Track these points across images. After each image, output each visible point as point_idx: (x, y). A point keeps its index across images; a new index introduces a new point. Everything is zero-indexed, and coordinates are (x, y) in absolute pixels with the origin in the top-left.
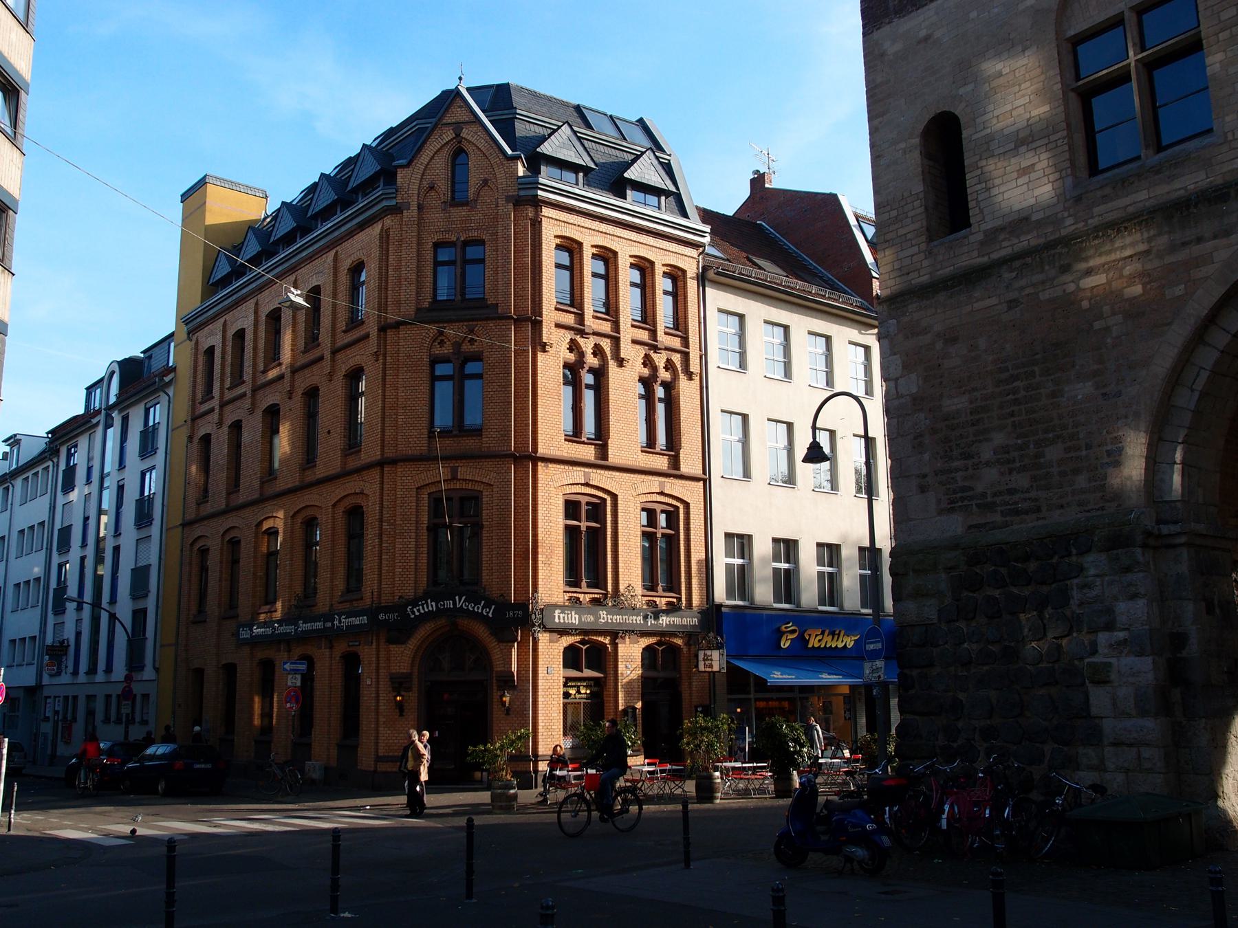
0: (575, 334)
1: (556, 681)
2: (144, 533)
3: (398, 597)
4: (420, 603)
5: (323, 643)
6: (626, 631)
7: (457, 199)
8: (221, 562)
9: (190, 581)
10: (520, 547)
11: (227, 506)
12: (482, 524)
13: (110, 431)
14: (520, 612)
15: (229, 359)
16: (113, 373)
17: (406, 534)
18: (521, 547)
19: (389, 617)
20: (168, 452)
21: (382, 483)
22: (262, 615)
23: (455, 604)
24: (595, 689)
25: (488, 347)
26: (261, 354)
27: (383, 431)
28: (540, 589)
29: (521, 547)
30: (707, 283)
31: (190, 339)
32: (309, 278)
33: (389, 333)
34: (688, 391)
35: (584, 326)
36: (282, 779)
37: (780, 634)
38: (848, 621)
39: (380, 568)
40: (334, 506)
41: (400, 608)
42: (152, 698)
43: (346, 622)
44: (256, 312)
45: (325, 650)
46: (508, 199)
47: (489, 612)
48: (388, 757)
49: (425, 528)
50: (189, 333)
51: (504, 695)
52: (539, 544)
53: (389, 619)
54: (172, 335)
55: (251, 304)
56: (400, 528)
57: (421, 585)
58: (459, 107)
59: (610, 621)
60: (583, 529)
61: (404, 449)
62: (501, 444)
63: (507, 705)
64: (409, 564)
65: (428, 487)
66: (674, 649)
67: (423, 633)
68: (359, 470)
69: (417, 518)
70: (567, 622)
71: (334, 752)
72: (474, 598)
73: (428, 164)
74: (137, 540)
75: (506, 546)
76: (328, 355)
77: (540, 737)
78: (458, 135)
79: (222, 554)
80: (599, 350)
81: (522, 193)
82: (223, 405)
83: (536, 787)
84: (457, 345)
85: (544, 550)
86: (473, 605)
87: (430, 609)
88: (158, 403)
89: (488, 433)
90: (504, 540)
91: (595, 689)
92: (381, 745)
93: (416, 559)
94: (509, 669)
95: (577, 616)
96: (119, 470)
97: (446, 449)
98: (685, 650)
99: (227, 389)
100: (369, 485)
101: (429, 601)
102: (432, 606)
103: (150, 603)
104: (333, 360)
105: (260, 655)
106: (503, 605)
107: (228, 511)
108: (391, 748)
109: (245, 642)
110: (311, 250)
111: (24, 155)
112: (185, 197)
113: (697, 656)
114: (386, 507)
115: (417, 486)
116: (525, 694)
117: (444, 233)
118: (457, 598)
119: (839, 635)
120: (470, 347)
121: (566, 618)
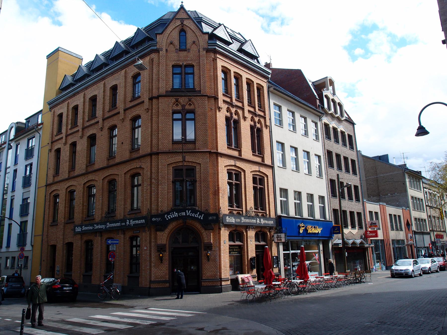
2: (27, 190)
3: (160, 211)
4: (171, 213)
5: (120, 232)
7: (183, 48)
8: (65, 200)
9: (49, 208)
11: (68, 177)
13: (10, 151)
14: (215, 217)
15: (70, 117)
16: (12, 127)
17: (163, 184)
19: (157, 219)
20: (39, 157)
21: (151, 162)
23: (186, 214)
26: (87, 114)
27: (152, 141)
31: (50, 111)
32: (111, 82)
33: (154, 101)
34: (266, 132)
35: (232, 102)
37: (299, 227)
38: (315, 223)
39: (151, 199)
40: (125, 174)
41: (162, 215)
42: (30, 258)
43: (132, 222)
44: (68, 106)
46: (204, 49)
47: (201, 217)
48: (156, 281)
49: (171, 182)
50: (50, 109)
52: (220, 189)
54: (41, 111)
55: (82, 95)
56: (160, 181)
58: (183, 12)
59: (245, 222)
64: (165, 197)
68: (138, 158)
73: (170, 34)
75: (207, 189)
76: (81, 130)
77: (222, 270)
78: (182, 23)
80: (237, 113)
81: (210, 47)
82: (67, 136)
85: (222, 192)
86: (194, 214)
87: (175, 216)
88: (34, 137)
90: (206, 187)
92: (153, 276)
95: (234, 219)
96: (14, 165)
99: (69, 129)
100: (145, 164)
101: (175, 212)
102: (176, 215)
103: (30, 218)
104: (125, 113)
105: (85, 238)
106: (207, 214)
107: (87, 173)
109: (79, 233)
110: (113, 70)
112: (48, 57)
115: (168, 164)
117: (177, 61)
118: (187, 211)
119: (316, 228)
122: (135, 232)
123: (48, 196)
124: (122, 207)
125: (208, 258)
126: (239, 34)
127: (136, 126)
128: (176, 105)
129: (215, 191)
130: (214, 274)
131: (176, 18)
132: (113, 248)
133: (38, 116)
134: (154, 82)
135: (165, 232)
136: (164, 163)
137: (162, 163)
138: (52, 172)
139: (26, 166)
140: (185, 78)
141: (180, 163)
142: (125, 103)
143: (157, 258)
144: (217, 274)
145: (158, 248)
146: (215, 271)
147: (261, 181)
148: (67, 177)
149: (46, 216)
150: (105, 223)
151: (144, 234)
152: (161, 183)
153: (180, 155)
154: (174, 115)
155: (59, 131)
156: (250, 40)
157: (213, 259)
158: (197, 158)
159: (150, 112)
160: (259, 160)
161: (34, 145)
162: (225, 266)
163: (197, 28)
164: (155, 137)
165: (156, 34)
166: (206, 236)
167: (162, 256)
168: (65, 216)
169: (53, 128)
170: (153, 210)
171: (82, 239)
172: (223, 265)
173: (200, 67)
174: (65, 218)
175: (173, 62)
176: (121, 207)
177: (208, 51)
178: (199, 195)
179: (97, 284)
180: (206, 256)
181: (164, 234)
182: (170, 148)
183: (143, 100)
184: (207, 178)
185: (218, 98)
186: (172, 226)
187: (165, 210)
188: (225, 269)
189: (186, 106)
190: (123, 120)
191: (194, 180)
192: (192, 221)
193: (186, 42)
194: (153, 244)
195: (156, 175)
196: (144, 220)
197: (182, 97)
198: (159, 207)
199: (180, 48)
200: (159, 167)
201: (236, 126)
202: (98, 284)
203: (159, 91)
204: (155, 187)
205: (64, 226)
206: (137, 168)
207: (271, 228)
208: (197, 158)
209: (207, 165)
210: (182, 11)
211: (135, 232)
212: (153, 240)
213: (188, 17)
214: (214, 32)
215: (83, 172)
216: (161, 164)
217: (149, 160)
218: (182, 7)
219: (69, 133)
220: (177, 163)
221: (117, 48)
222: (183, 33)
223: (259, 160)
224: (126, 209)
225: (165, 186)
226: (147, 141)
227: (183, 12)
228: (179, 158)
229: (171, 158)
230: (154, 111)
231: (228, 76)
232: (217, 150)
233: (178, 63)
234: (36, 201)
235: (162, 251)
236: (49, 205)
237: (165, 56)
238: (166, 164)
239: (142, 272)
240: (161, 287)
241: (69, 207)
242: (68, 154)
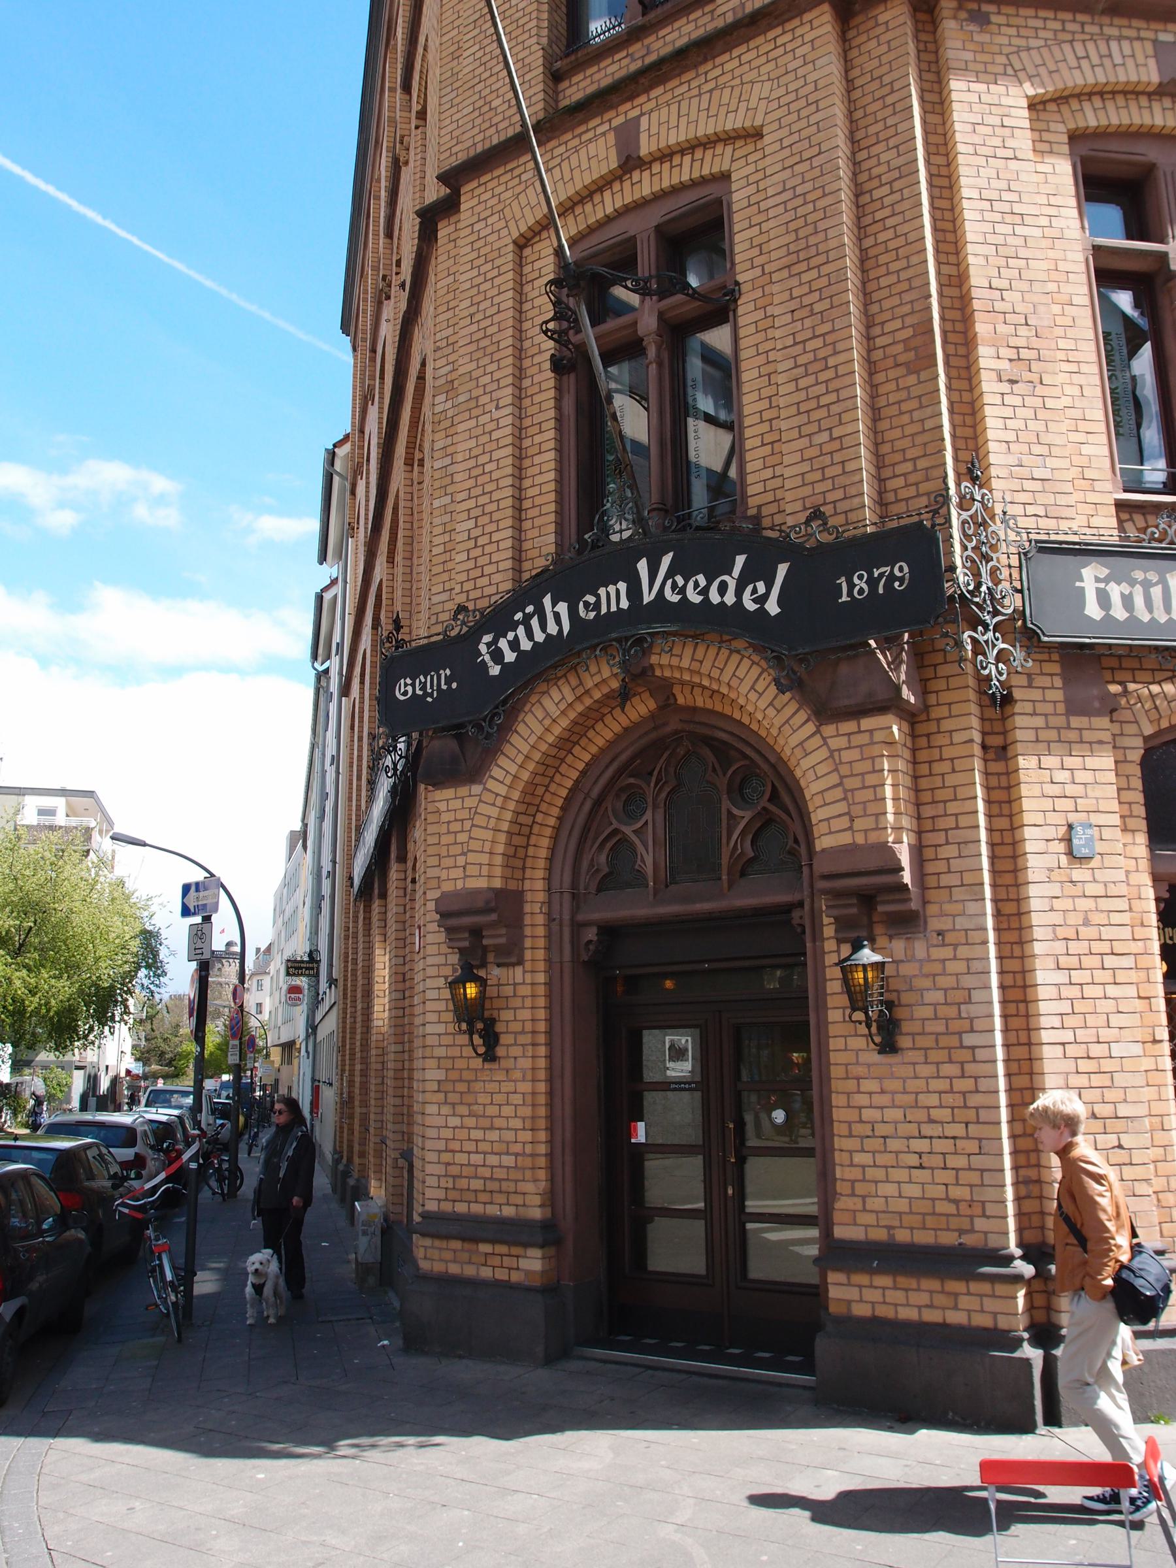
1: (1123, 889)
4: (519, 616)
12: (737, 284)
14: (901, 569)
19: (423, 688)
23: (634, 592)
28: (997, 458)
49: (547, 365)
53: (426, 694)
70: (1146, 617)
83: (616, 832)
101: (547, 601)
102: (557, 616)
116: (963, 951)
118: (642, 566)
121: (1139, 601)
130: (955, 1192)
135: (491, 784)
146: (961, 1162)
157: (940, 1027)
166: (834, 779)
172: (439, 1170)
240: (486, 1273)
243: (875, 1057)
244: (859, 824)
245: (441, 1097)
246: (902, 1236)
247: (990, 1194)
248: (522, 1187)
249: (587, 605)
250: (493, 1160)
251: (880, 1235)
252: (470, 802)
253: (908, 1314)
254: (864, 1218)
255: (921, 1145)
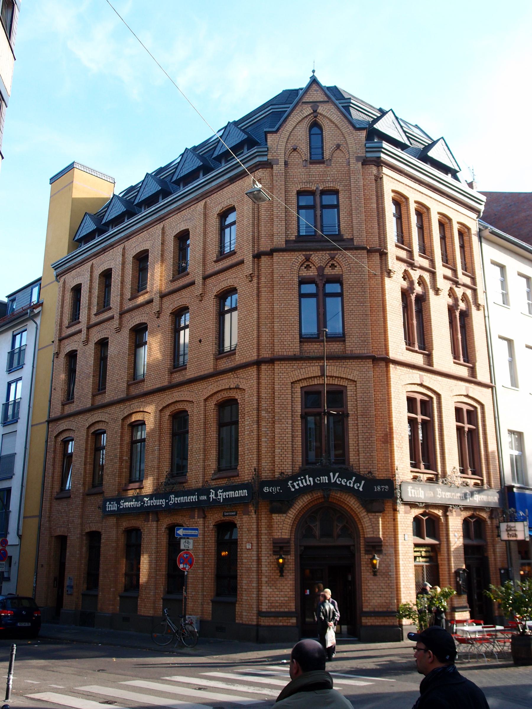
0: (407, 266)
4: (299, 478)
5: (196, 513)
6: (454, 505)
8: (86, 450)
9: (54, 465)
10: (379, 432)
11: (92, 405)
14: (387, 487)
15: (96, 292)
18: (381, 432)
19: (272, 490)
21: (259, 378)
22: (130, 491)
24: (432, 554)
25: (347, 271)
27: (259, 337)
29: (381, 432)
30: (483, 240)
31: (57, 281)
33: (264, 259)
34: (476, 317)
35: (414, 260)
36: (177, 632)
40: (206, 400)
42: (15, 559)
43: (222, 495)
44: (92, 272)
45: (199, 520)
46: (358, 159)
49: (299, 416)
50: (57, 276)
51: (374, 558)
54: (40, 279)
55: (119, 249)
57: (297, 463)
58: (315, 90)
60: (420, 421)
61: (280, 350)
62: (362, 348)
63: (377, 567)
64: (287, 445)
65: (300, 382)
66: (480, 522)
67: (302, 504)
69: (292, 407)
71: (209, 608)
72: (347, 474)
73: (291, 132)
74: (3, 435)
75: (369, 431)
76: (117, 316)
78: (315, 111)
79: (87, 443)
80: (422, 281)
81: (369, 155)
84: (321, 269)
87: (308, 483)
88: (26, 330)
89: (350, 339)
90: (368, 426)
91: (432, 554)
92: (264, 601)
93: (292, 442)
94: (378, 536)
97: (314, 352)
98: (489, 522)
101: (307, 476)
102: (310, 481)
104: (204, 284)
105: (125, 524)
108: (273, 604)
109: (112, 513)
111: (15, 59)
113: (498, 527)
114: (264, 398)
115: (292, 381)
116: (389, 557)
118: (331, 474)
120: (332, 271)
122: (227, 514)
123: (51, 441)
124: (201, 464)
125: (375, 571)
126: (416, 126)
127: (226, 309)
128: (305, 268)
129: (386, 435)
131: (304, 100)
132: (187, 545)
133: (32, 289)
134: (262, 224)
135: (288, 514)
136: (285, 379)
137: (280, 379)
138: (59, 396)
139: (9, 384)
140: (321, 216)
141: (337, 379)
142: (204, 265)
143: (272, 566)
144: (393, 601)
145: (274, 546)
147: (472, 416)
148: (89, 405)
149: (48, 480)
150: (165, 496)
151: (246, 519)
152: (280, 418)
153: (316, 364)
154: (303, 286)
155: (75, 317)
156: (442, 138)
158: (348, 370)
159: (255, 280)
160: (463, 372)
161: (26, 345)
162: (408, 586)
163: (344, 119)
164: (266, 329)
165: (266, 133)
166: (370, 524)
167: (283, 563)
168: (85, 480)
169: (62, 312)
170: (264, 472)
171: (118, 526)
173: (351, 194)
174: (84, 484)
175: (299, 186)
176: (199, 464)
177: (365, 162)
178: (354, 442)
179: (149, 615)
180: (370, 565)
181: (286, 520)
182: (295, 350)
183: (240, 258)
184: (369, 409)
185: (386, 254)
186: (356, 507)
187: (287, 471)
188: (408, 592)
189: (326, 269)
190: (201, 297)
191: (343, 413)
192: (342, 494)
193: (322, 147)
194: (264, 538)
195: (268, 403)
196: (246, 491)
197: (318, 253)
198: (276, 466)
199: (310, 158)
200: (275, 386)
201: (421, 307)
202: (151, 615)
203: (272, 241)
204: (267, 427)
205: (84, 500)
206: (230, 389)
207: (492, 511)
208: (348, 370)
209: (368, 384)
210: (315, 87)
211: (227, 514)
212: (264, 531)
213: (326, 99)
214: (375, 126)
215: (122, 396)
216: (279, 382)
217: (255, 373)
218: (314, 81)
219: (94, 322)
220: (310, 380)
221: (187, 161)
222: (315, 130)
223: (463, 372)
224: (208, 468)
225: (287, 425)
226: (251, 338)
227: (315, 90)
228: (313, 370)
229: (298, 371)
230: (263, 279)
231: (403, 209)
232: (387, 354)
233: (332, 185)
234: (28, 451)
235: (282, 553)
236: (54, 458)
237: (284, 174)
238: (289, 382)
239: (242, 594)
240: (281, 624)
241: (93, 463)
242: (91, 361)
243: (372, 576)
244: (375, 533)
245: (267, 585)
246: (377, 610)
247: (393, 601)
248: (290, 604)
249: (317, 480)
250: (282, 599)
251: (372, 610)
252: (282, 518)
253: (378, 624)
254: (369, 607)
255: (380, 593)
